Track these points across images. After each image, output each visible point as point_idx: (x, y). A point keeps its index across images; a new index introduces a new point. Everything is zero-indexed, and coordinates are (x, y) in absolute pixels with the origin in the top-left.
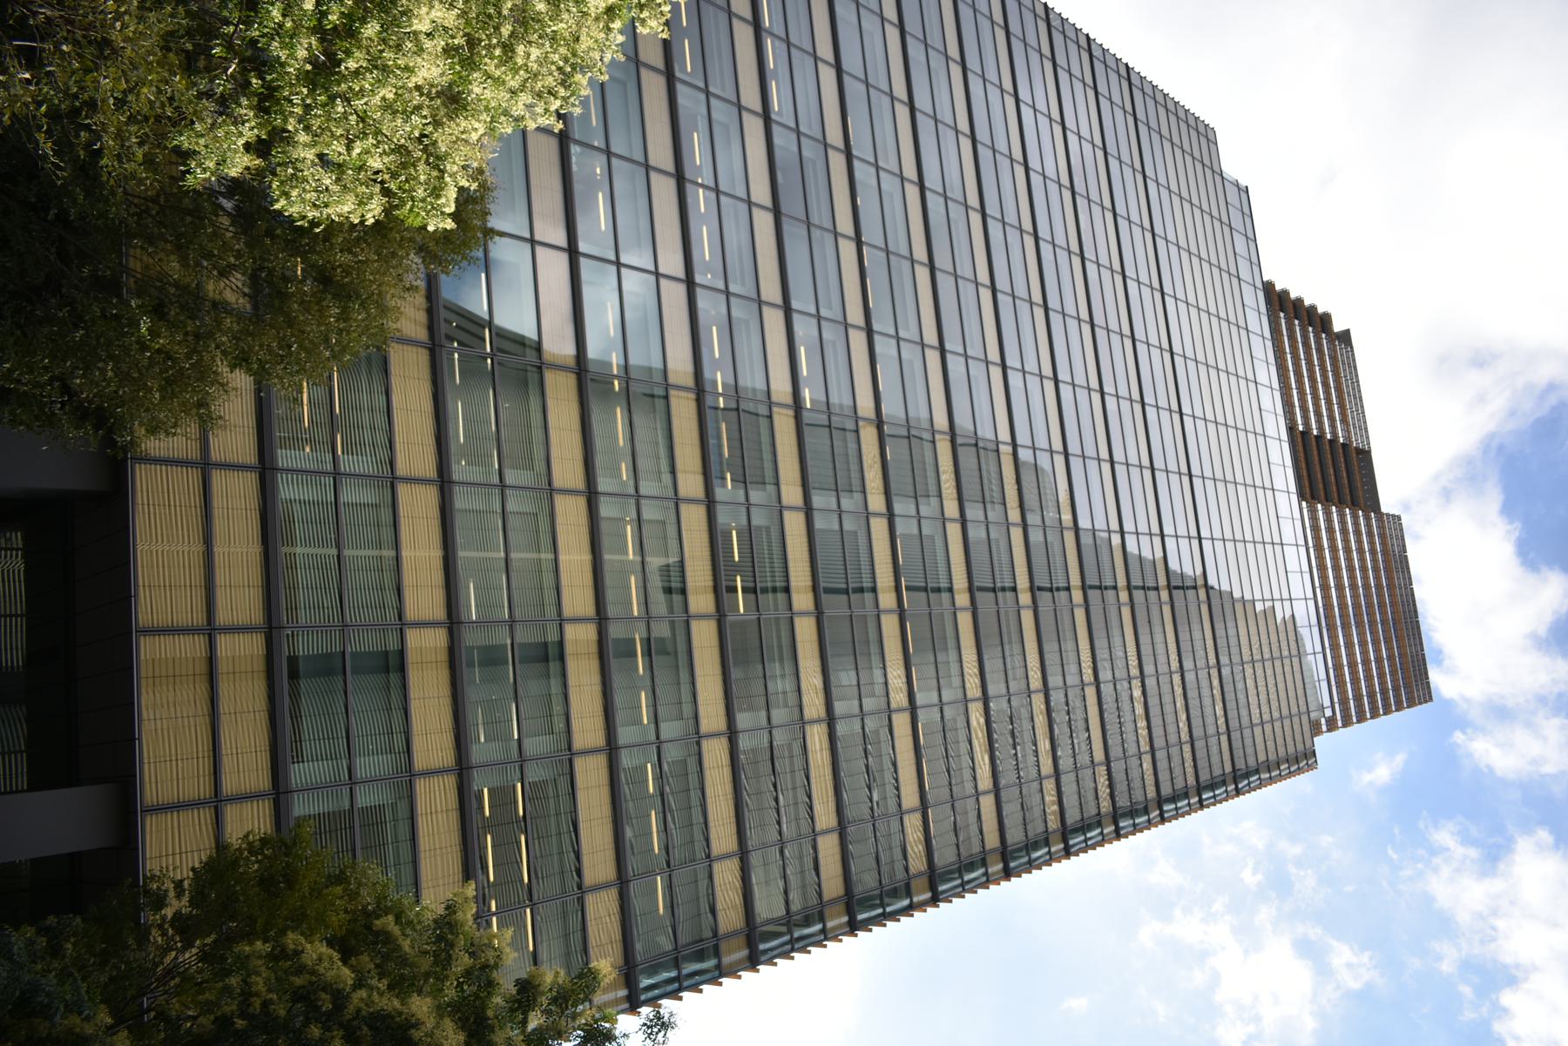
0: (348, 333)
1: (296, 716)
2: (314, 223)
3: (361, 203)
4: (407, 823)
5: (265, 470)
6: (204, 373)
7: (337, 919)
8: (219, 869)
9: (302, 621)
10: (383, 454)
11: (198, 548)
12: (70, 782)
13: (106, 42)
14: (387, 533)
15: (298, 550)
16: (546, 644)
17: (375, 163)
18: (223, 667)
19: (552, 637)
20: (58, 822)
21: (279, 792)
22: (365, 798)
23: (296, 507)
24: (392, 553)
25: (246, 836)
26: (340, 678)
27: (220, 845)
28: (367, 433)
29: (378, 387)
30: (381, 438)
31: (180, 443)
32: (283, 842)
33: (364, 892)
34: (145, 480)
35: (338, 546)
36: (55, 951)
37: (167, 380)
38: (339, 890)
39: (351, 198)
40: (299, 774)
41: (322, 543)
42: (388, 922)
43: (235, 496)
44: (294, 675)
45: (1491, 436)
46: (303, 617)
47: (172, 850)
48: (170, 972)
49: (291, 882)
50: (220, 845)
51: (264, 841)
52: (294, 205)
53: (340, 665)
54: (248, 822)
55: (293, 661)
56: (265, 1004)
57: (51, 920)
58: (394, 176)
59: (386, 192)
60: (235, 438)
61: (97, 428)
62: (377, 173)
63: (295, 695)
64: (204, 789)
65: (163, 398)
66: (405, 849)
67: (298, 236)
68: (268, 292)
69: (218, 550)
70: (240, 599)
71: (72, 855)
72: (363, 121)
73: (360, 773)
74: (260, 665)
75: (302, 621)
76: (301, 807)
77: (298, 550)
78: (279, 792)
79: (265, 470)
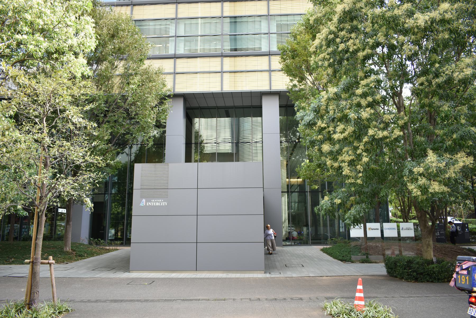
0: (129, 29)
1: (247, 49)
2: (97, 38)
3: (88, 23)
4: (282, 17)
5: (175, 57)
6: (146, 72)
7: (307, 37)
8: (288, 70)
9: (220, 47)
10: (168, 22)
11: (198, 59)
12: (261, 107)
13: (52, 92)
14: (194, 21)
15: (199, 48)
16: (230, 22)
17: (73, 18)
18: (233, 69)
19: (228, 20)
20: (271, 109)
21: (269, 54)
22: (274, 29)
23: (186, 48)
24: (200, 19)
25: (280, 63)
26: (237, 36)
27: (282, 70)
28: (162, 27)
29: (147, 23)
30: (164, 22)
31: (169, 81)
32: (283, 53)
33: (300, 29)
34: (180, 89)
35: (198, 36)
36: (303, 108)
37: (150, 82)
38: (298, 37)
39: (86, 26)
40: (265, 49)
41: (197, 41)
42: (312, 19)
43: (182, 65)
44: (236, 50)
45: (165, 156)
46: (219, 47)
47: (282, 82)
48: (313, 84)
49: (294, 51)
50: (282, 70)
51: (282, 58)
52: (92, 44)
53: (233, 36)
54: (277, 63)
55: (231, 50)
56: (328, 54)
57: (296, 109)
58: (77, 12)
59: (83, 14)
60: (167, 65)
61: (165, 99)
62: (76, 18)
63: (241, 50)
64: (267, 74)
65: (155, 82)
66: (289, 18)
67: (101, 45)
68: (120, 53)
69: (199, 70)
70: (214, 64)
71: (280, 107)
72: (60, 22)
73: (266, 31)
74: (233, 59)
75: (220, 47)
76: (274, 48)
77: (199, 48)
78: (269, 54)
79: (175, 57)
